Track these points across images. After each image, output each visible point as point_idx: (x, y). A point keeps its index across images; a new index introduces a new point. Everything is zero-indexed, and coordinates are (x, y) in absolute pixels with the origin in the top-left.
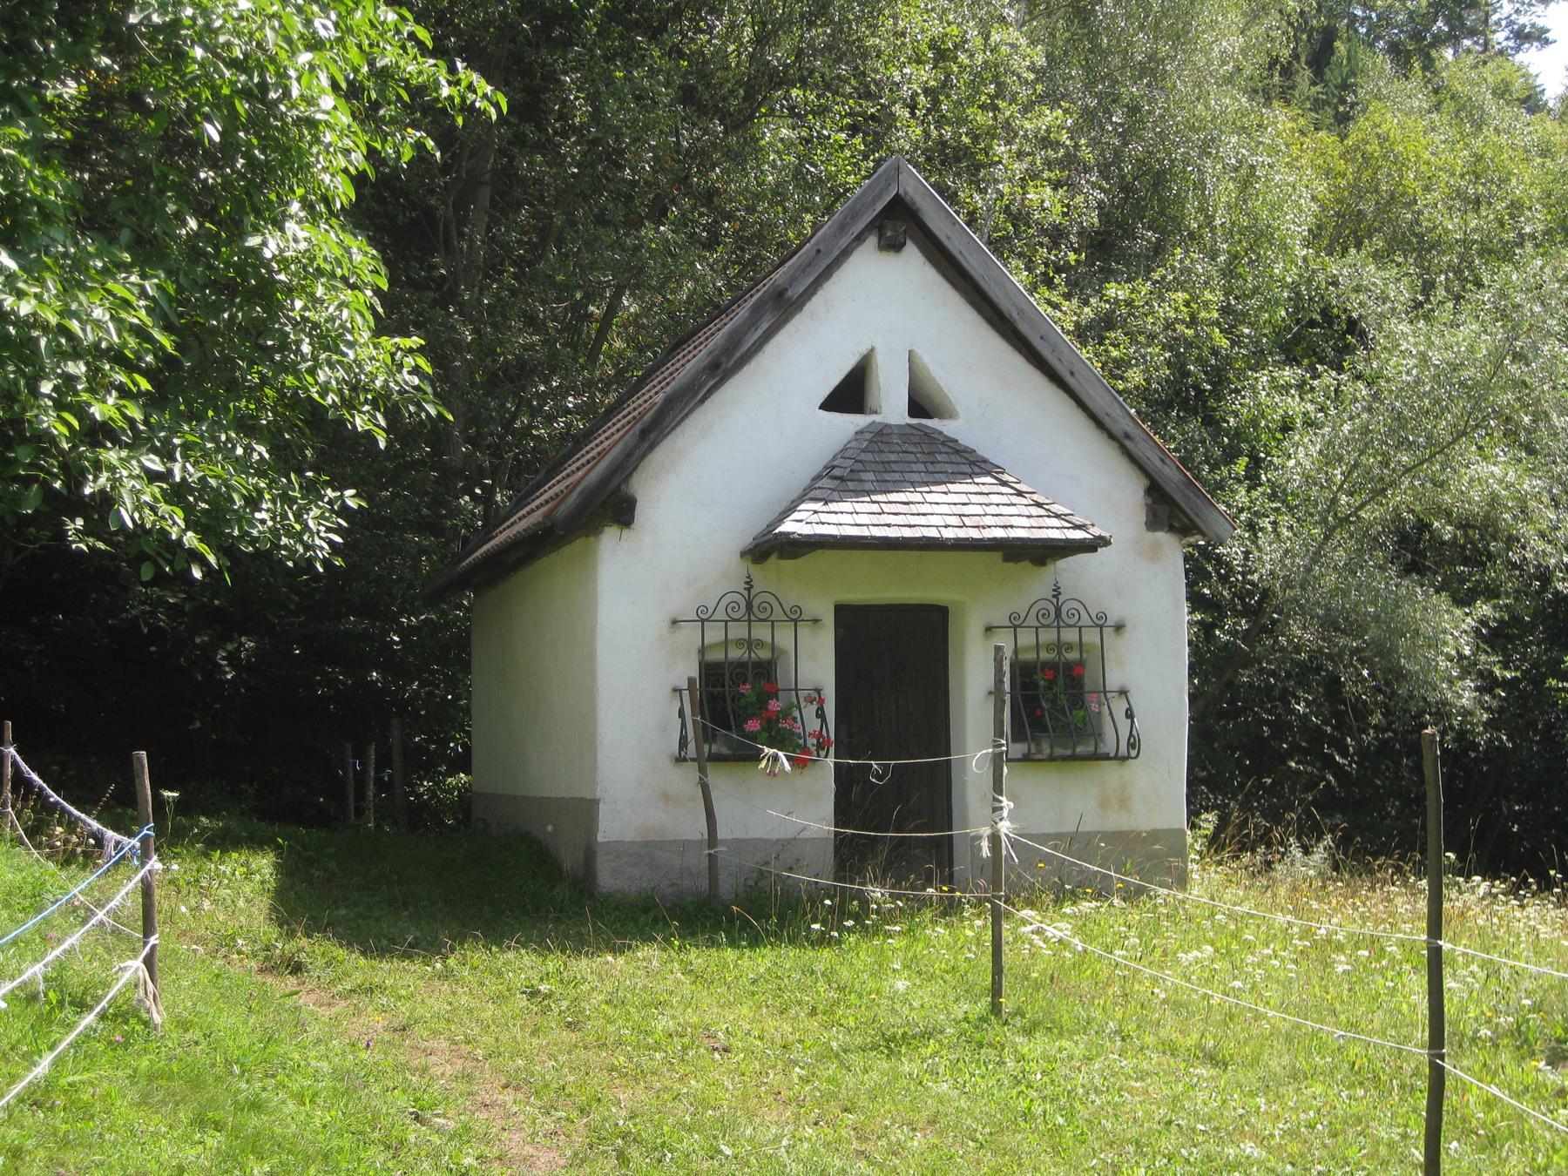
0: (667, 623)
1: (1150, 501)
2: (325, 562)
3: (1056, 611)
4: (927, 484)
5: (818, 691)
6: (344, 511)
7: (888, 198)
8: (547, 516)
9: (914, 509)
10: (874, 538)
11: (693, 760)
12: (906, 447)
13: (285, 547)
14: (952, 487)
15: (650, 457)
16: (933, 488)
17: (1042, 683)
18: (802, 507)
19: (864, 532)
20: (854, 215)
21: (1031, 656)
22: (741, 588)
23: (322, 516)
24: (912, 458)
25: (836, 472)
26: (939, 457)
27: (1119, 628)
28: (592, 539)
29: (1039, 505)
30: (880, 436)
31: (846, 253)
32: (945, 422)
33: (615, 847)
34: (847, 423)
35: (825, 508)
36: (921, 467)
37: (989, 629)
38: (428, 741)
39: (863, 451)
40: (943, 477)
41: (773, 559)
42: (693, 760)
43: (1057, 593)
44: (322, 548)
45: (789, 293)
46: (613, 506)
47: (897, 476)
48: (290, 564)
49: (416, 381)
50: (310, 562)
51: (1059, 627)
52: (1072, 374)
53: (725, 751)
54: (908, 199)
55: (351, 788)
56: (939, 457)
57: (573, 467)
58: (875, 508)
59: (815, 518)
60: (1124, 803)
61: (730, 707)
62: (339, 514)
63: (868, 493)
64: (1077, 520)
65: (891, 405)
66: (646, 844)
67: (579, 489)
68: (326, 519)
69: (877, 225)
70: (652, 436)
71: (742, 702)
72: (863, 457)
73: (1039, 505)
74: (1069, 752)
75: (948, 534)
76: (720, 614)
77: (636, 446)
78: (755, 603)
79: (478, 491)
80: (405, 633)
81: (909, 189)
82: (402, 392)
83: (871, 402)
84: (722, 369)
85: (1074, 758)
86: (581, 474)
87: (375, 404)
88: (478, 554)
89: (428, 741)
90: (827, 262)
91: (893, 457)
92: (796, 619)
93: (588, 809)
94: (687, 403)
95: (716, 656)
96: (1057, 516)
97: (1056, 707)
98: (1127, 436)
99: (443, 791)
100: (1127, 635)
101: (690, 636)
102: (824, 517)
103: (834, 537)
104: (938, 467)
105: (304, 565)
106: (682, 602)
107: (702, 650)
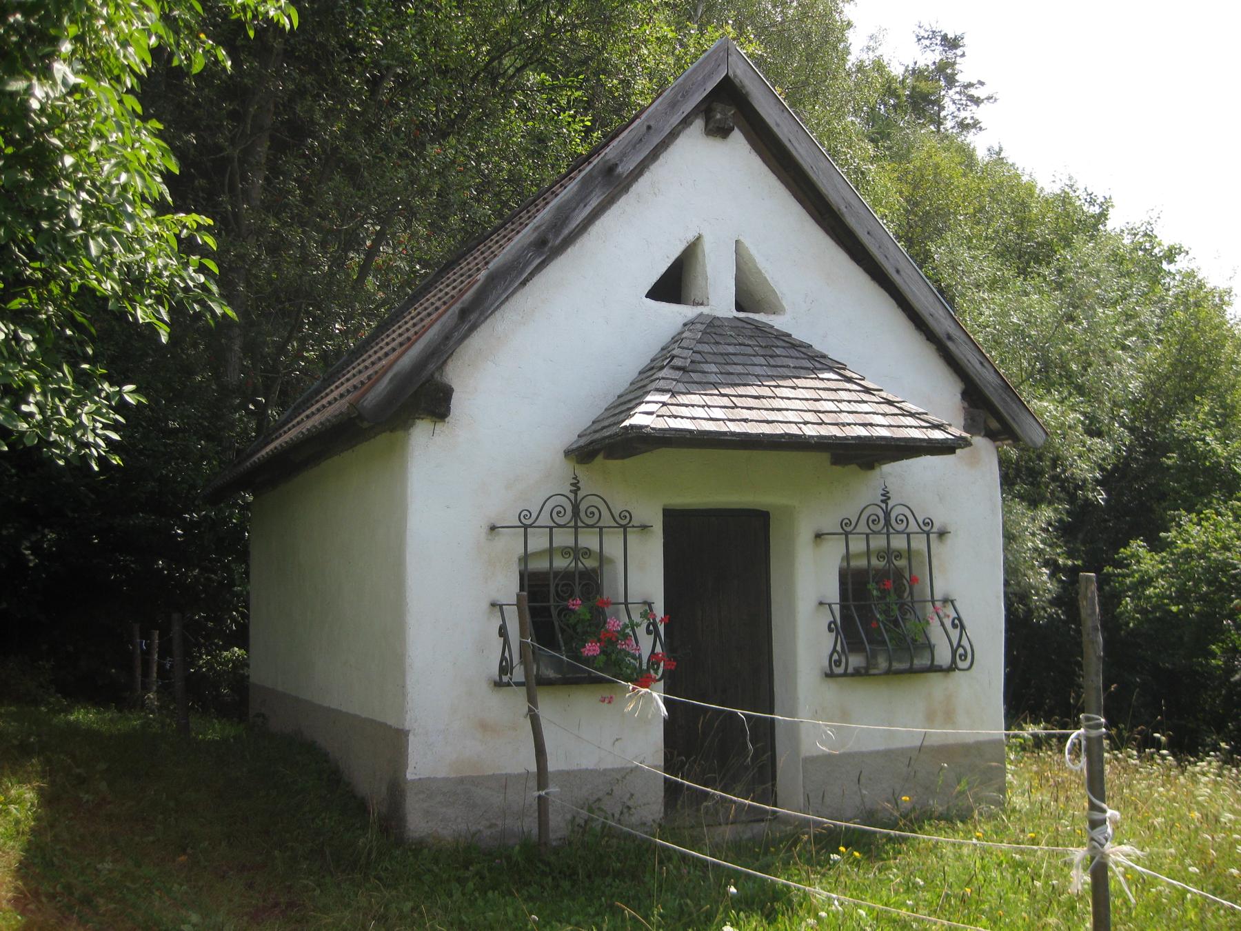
0: (485, 530)
1: (966, 405)
2: (101, 460)
3: (886, 517)
4: (772, 378)
5: (650, 605)
6: (122, 407)
7: (718, 79)
8: (352, 405)
9: (766, 403)
10: (733, 434)
11: (518, 684)
12: (741, 340)
13: (55, 444)
14: (799, 382)
15: (466, 342)
16: (781, 383)
17: (875, 593)
18: (648, 398)
19: (722, 427)
20: (684, 93)
21: (862, 563)
22: (567, 489)
23: (98, 412)
24: (749, 350)
25: (677, 362)
26: (778, 351)
27: (942, 534)
28: (400, 434)
29: (890, 403)
30: (712, 327)
31: (673, 135)
32: (772, 317)
33: (426, 784)
34: (673, 315)
35: (674, 401)
36: (762, 360)
37: (818, 536)
38: (207, 619)
39: (700, 342)
40: (787, 372)
41: (599, 459)
42: (518, 684)
43: (886, 497)
44: (97, 446)
45: (620, 169)
46: (428, 398)
47: (739, 369)
48: (61, 463)
49: (202, 279)
50: (85, 459)
51: (888, 535)
52: (898, 272)
53: (550, 674)
54: (737, 81)
55: (138, 663)
56: (778, 351)
57: (336, 394)
58: (725, 401)
59: (664, 411)
60: (949, 717)
61: (558, 628)
62: (116, 410)
63: (715, 385)
64: (932, 418)
65: (718, 296)
66: (461, 781)
67: (390, 375)
68: (102, 415)
69: (705, 110)
70: (473, 317)
71: (572, 620)
72: (700, 347)
73: (890, 403)
74: (905, 666)
75: (810, 431)
76: (544, 520)
77: (456, 328)
78: (583, 507)
79: (251, 407)
80: (188, 526)
81: (739, 72)
82: (187, 289)
83: (696, 294)
84: (549, 247)
85: (912, 671)
86: (397, 356)
87: (159, 300)
88: (263, 453)
89: (207, 619)
90: (656, 140)
91: (731, 349)
92: (625, 524)
93: (396, 739)
94: (512, 281)
95: (541, 565)
96: (912, 415)
97: (884, 621)
98: (949, 338)
99: (220, 664)
100: (949, 539)
101: (512, 545)
102: (675, 410)
103: (691, 431)
104: (779, 361)
105: (76, 462)
106: (503, 506)
107: (525, 558)
